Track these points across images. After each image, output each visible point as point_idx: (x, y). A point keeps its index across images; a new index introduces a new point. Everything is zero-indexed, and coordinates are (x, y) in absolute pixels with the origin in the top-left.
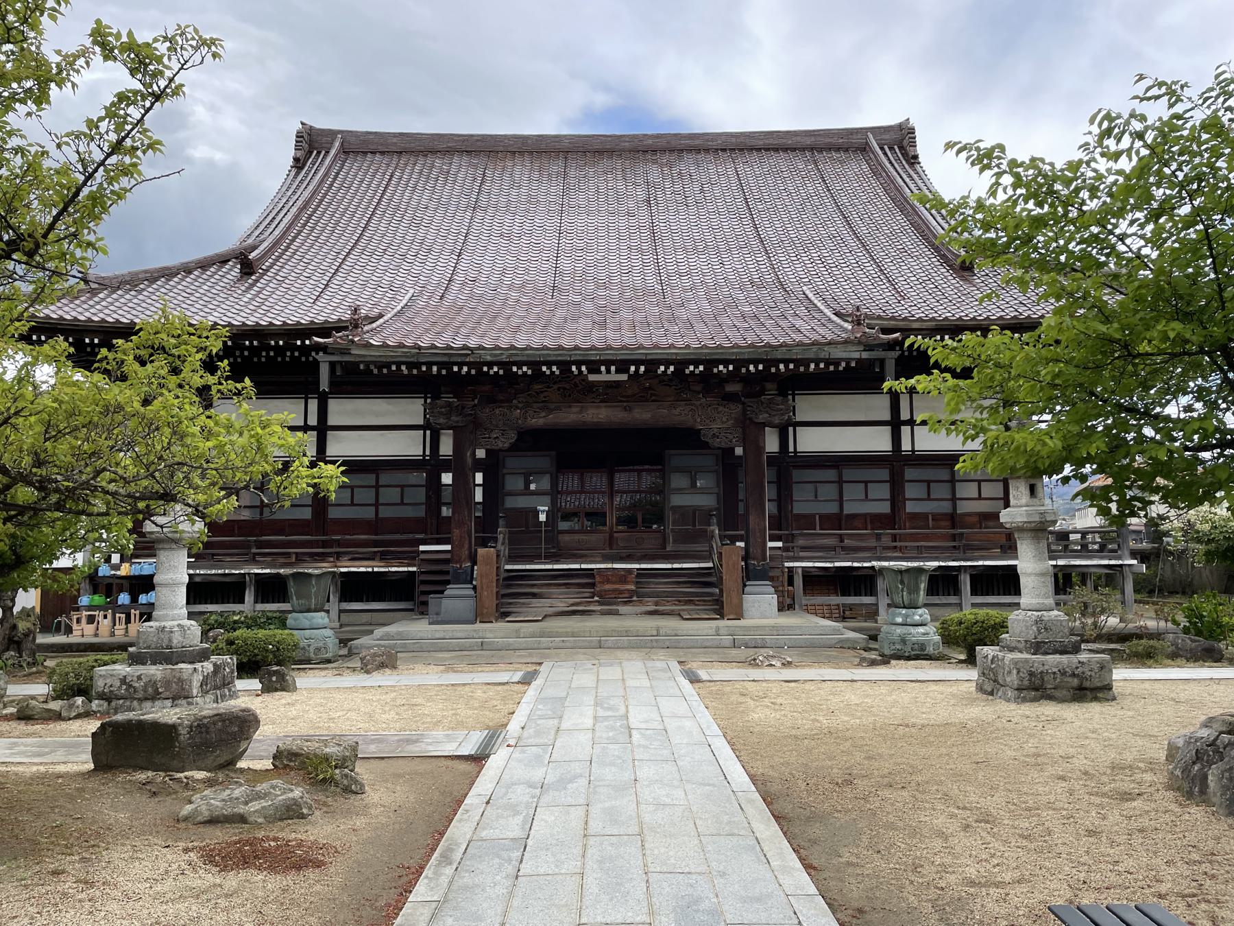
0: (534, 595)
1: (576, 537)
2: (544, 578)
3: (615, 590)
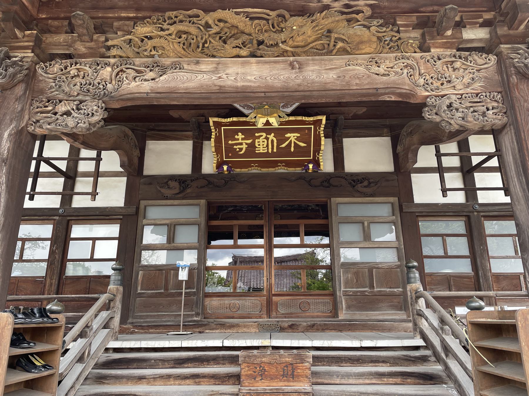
1: (227, 301)
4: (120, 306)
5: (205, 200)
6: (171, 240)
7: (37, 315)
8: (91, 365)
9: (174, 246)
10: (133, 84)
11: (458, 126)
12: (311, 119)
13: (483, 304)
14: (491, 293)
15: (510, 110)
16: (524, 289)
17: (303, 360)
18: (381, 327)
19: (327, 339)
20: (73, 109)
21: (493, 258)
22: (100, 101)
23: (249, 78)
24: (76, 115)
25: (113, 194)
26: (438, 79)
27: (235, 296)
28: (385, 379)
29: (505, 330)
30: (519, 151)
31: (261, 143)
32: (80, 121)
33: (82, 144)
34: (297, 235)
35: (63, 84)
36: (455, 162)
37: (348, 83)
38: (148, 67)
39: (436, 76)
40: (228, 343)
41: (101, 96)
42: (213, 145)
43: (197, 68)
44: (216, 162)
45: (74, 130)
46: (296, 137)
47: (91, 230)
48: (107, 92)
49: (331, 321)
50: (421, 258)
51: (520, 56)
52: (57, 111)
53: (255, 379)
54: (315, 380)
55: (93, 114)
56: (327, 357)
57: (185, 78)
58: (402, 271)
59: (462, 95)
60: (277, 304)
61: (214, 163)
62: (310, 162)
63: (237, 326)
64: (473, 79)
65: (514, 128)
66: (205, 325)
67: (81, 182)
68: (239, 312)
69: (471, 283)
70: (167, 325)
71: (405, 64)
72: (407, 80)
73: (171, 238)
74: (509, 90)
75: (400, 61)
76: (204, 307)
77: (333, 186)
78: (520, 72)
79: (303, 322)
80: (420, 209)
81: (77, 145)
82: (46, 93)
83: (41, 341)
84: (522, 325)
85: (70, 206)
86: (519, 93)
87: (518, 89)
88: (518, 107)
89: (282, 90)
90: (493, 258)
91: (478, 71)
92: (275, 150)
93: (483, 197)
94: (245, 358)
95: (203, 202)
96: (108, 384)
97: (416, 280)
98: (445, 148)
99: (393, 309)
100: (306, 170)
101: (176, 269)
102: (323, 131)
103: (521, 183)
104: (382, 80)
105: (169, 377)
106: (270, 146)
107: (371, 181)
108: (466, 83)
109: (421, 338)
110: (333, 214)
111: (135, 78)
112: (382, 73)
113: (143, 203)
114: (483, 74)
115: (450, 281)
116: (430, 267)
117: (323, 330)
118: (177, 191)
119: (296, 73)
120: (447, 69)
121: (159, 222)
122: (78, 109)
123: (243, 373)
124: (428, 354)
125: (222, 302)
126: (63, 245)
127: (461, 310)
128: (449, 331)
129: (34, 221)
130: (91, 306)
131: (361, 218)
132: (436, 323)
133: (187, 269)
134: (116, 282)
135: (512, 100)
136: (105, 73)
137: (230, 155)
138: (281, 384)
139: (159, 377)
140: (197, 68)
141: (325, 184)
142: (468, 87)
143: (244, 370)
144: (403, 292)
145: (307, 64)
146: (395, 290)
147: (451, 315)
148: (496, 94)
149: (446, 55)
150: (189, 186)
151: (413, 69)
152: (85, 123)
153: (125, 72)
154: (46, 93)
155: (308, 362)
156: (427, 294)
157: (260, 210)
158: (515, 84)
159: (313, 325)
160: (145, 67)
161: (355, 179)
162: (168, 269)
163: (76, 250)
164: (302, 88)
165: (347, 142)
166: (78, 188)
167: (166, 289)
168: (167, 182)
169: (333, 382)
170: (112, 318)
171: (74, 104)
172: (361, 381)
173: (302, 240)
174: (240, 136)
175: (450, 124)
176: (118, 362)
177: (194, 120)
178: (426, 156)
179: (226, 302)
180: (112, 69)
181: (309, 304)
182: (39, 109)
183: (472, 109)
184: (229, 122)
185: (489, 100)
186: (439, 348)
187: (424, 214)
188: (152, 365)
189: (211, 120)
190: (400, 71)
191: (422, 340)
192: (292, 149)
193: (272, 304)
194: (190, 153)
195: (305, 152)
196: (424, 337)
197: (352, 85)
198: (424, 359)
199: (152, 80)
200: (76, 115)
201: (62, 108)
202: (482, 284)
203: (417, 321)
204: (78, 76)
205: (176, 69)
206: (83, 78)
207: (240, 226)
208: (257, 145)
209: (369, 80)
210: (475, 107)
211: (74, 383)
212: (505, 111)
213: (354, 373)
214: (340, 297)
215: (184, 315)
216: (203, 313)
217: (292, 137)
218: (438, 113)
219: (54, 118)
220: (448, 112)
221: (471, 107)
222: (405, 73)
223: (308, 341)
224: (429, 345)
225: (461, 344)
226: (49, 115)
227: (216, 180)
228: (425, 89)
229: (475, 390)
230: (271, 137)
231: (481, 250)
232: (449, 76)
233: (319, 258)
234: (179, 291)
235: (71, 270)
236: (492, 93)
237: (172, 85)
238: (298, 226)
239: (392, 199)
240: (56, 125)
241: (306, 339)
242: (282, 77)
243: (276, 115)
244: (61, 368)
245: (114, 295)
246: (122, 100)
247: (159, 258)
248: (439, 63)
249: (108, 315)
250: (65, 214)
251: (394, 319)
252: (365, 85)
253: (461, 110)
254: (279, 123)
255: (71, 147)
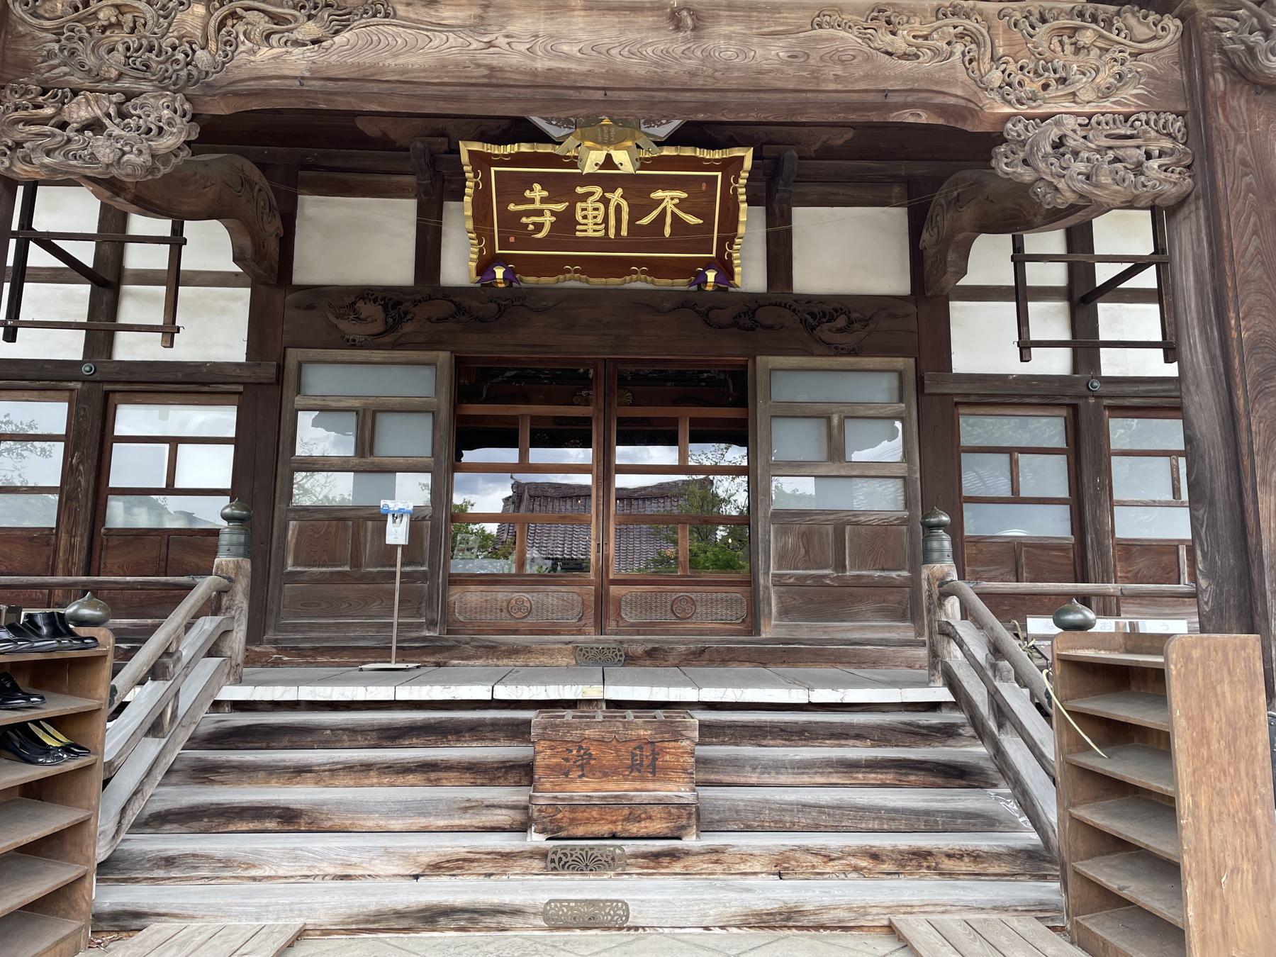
0: (288, 819)
1: (502, 594)
2: (354, 736)
3: (607, 805)
4: (245, 606)
5: (448, 354)
6: (367, 448)
7: (45, 630)
8: (179, 740)
9: (373, 463)
10: (265, 53)
11: (1074, 196)
12: (717, 154)
13: (1091, 615)
14: (1111, 587)
15: (1201, 159)
16: (1185, 577)
17: (676, 734)
18: (855, 656)
19: (733, 686)
20: (109, 116)
21: (1123, 504)
22: (179, 96)
23: (565, 48)
24: (117, 132)
25: (217, 329)
26: (1036, 72)
27: (521, 583)
28: (860, 776)
29: (1144, 681)
30: (1212, 264)
31: (590, 213)
32: (127, 149)
33: (133, 202)
34: (669, 439)
35: (79, 46)
36: (1055, 275)
37: (816, 75)
38: (303, 7)
39: (1031, 66)
40: (503, 693)
41: (181, 83)
42: (469, 213)
43: (431, 16)
44: (475, 257)
45: (114, 172)
46: (677, 201)
47: (164, 417)
48: (195, 73)
49: (743, 642)
50: (955, 501)
51: (1237, 24)
52: (66, 119)
53: (566, 775)
54: (702, 776)
55: (161, 129)
56: (732, 726)
57: (400, 41)
58: (912, 532)
59: (1090, 116)
60: (619, 601)
61: (472, 260)
62: (709, 265)
63: (526, 650)
64: (1121, 76)
65: (1206, 207)
66: (450, 648)
67: (132, 295)
68: (530, 620)
69: (1066, 561)
70: (358, 648)
71: (960, 29)
72: (961, 74)
73: (365, 444)
74: (1204, 109)
75: (947, 21)
76: (447, 607)
77: (764, 327)
78: (1233, 66)
79: (677, 643)
80: (965, 388)
81: (120, 203)
82: (37, 71)
83: (57, 690)
84: (1179, 673)
85: (110, 356)
86: (1226, 118)
87: (1224, 109)
88: (1221, 155)
89: (648, 85)
90: (1123, 504)
91: (1135, 55)
92: (624, 233)
93: (1113, 364)
94: (545, 728)
95: (444, 357)
96: (222, 783)
97: (942, 556)
98: (1036, 242)
99: (886, 616)
100: (699, 285)
101: (380, 519)
102: (746, 186)
103: (1207, 341)
104: (898, 71)
105: (366, 767)
106: (612, 222)
107: (854, 315)
108: (1103, 88)
109: (944, 685)
110: (759, 395)
111: (268, 37)
112: (900, 52)
113: (293, 355)
114: (1145, 64)
115: (1018, 557)
116: (976, 522)
117: (724, 662)
118: (378, 327)
119: (686, 41)
120: (1059, 49)
121: (334, 404)
122: (123, 115)
123: (539, 761)
124: (959, 721)
125: (490, 596)
126: (96, 454)
127: (1040, 625)
128: (1009, 671)
129: (20, 393)
130: (176, 601)
131: (825, 407)
132: (981, 654)
133: (406, 519)
134: (233, 548)
135: (1208, 136)
136: (189, 19)
137: (512, 239)
138: (627, 785)
139: (343, 769)
140: (431, 16)
141: (745, 321)
142: (1105, 97)
143: (544, 757)
144: (911, 578)
145: (716, 19)
146: (894, 574)
147: (1017, 635)
148: (1171, 117)
149: (1062, 11)
150: (409, 317)
151: (978, 45)
152: (140, 152)
153: (241, 18)
154: (37, 71)
155: (688, 738)
156: (966, 587)
157: (585, 381)
158: (1219, 94)
159: (702, 651)
160: (294, 8)
161: (816, 310)
162: (359, 518)
163: (128, 467)
164: (699, 82)
165: (803, 217)
166: (129, 312)
167: (356, 563)
168: (354, 303)
169: (742, 780)
170: (226, 633)
171: (110, 102)
172: (805, 779)
173: (683, 455)
174: (538, 192)
175: (1057, 189)
176: (245, 733)
177: (419, 145)
178: (989, 259)
179: (500, 596)
180: (208, 9)
181: (693, 602)
182: (21, 114)
183: (1111, 154)
184: (510, 154)
185: (1153, 134)
186: (984, 708)
187: (972, 399)
188: (327, 742)
189: (465, 148)
190: (945, 46)
191: (946, 690)
192: (667, 231)
193: (608, 603)
194: (411, 232)
195: (696, 238)
196: (952, 682)
197: (825, 80)
198: (948, 732)
199: (314, 42)
200: (117, 132)
201: (79, 111)
202: (1090, 563)
203: (940, 647)
204: (119, 24)
205: (374, 16)
206: (132, 32)
207: (534, 419)
208: (579, 218)
209: (867, 67)
210: (1119, 148)
211: (142, 783)
212: (1188, 162)
213: (792, 761)
214: (767, 588)
215: (399, 624)
216: (445, 621)
217: (669, 199)
218: (1030, 161)
219: (59, 139)
220: (1053, 160)
221: (1110, 148)
222: (958, 55)
223: (689, 689)
224: (961, 700)
225: (1032, 700)
226: (47, 128)
227: (475, 304)
228: (1003, 98)
229: (1059, 804)
230: (616, 197)
231: (1095, 487)
232: (1064, 66)
233: (721, 493)
234: (387, 569)
235: (119, 514)
236: (1162, 116)
237: (367, 58)
238: (675, 421)
239: (899, 362)
240: (66, 155)
241: (684, 684)
242: (649, 50)
243: (629, 143)
244: (112, 748)
245: (230, 579)
246: (237, 94)
247: (334, 489)
248: (1042, 30)
249: (218, 626)
250: (97, 377)
251: (887, 640)
252: (856, 81)
253: (1084, 155)
254: (638, 164)
255: (105, 209)
